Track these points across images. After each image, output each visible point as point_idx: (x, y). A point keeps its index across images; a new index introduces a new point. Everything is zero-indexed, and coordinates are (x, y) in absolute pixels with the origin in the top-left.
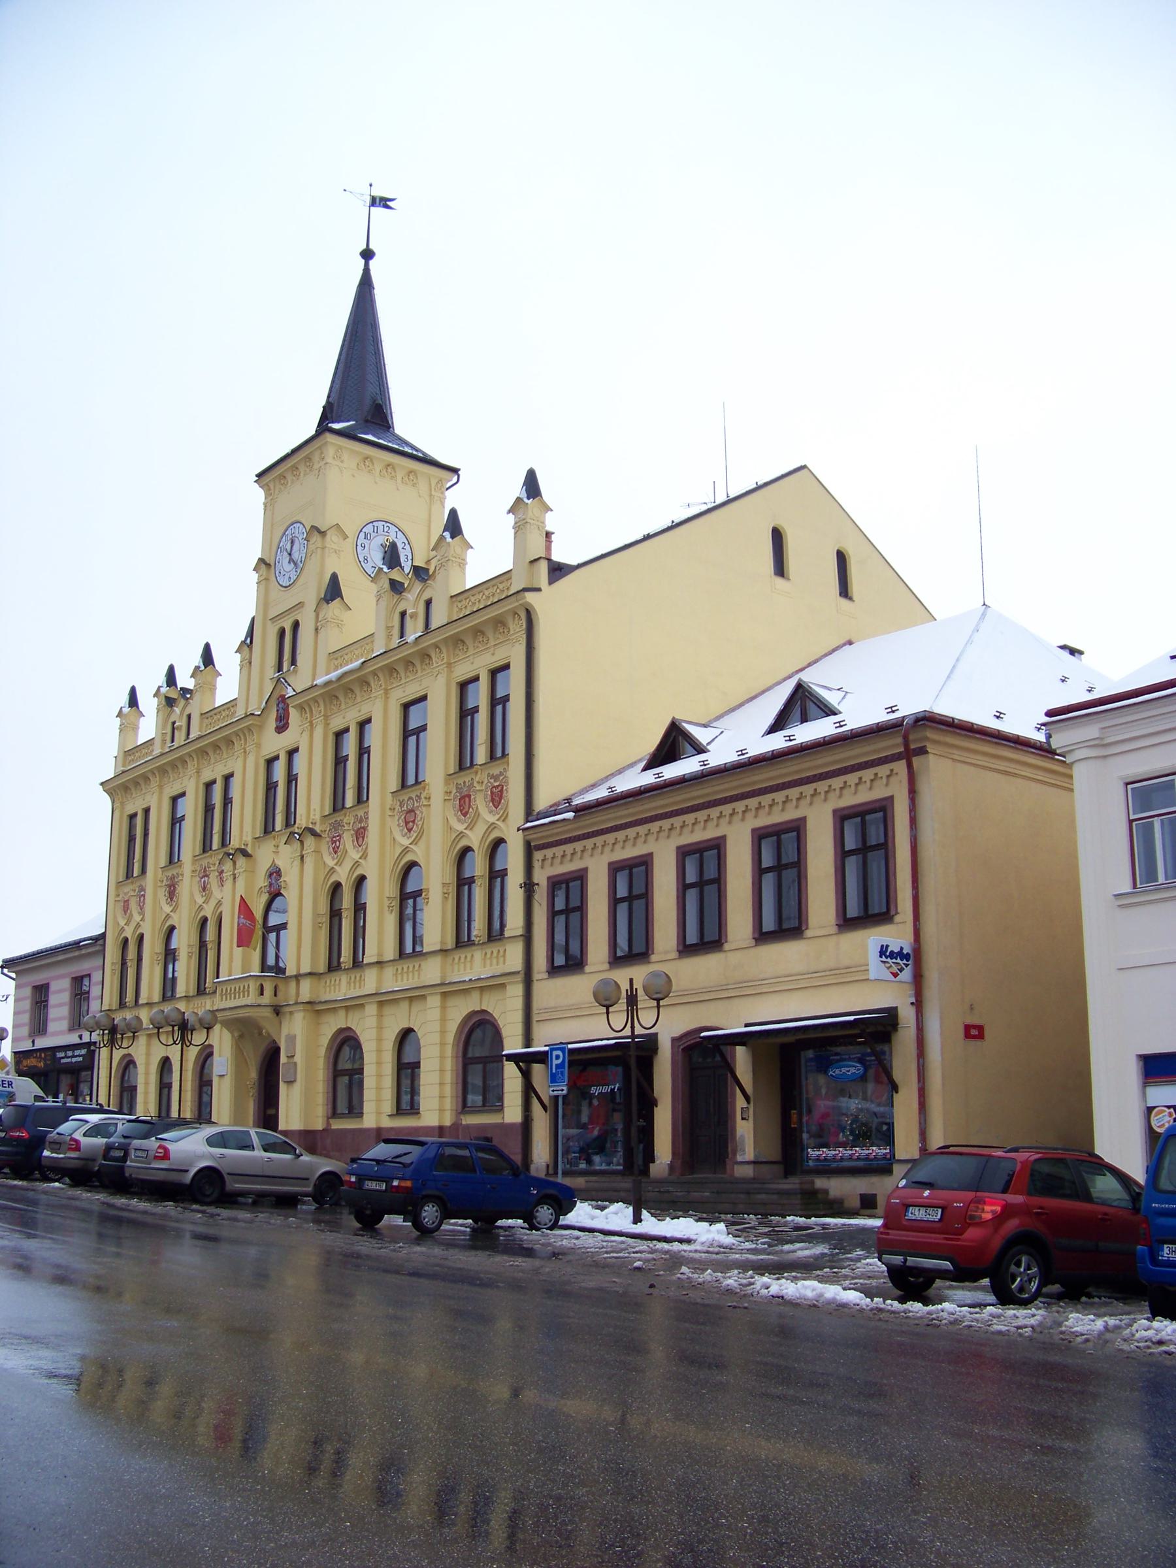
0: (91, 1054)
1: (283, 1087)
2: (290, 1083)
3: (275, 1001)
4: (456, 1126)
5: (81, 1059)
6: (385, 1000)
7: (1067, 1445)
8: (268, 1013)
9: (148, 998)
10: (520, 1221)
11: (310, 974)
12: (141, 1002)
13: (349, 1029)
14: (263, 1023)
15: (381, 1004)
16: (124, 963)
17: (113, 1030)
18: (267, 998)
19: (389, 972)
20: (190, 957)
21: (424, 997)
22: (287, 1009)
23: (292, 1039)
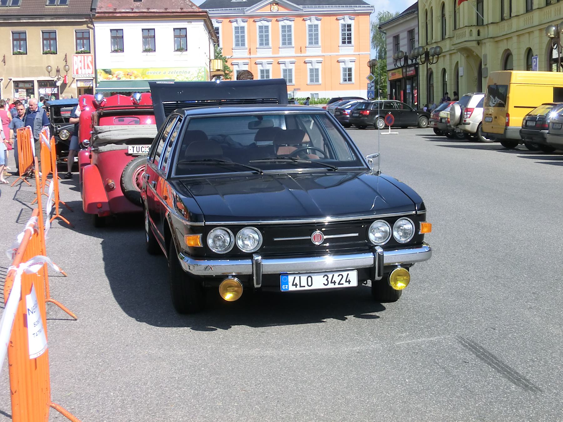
0: (417, 70)
1: (483, 79)
2: (486, 77)
3: (479, 38)
4: (254, 145)
5: (412, 72)
6: (520, 34)
7: (144, 196)
8: (474, 44)
9: (539, 4)
10: (499, 144)
11: (492, 23)
12: (512, 15)
13: (508, 49)
14: (473, 49)
15: (519, 36)
16: (443, 15)
17: (427, 54)
18: (475, 36)
19: (522, 19)
20: (450, 17)
21: (511, 37)
22: (484, 41)
23: (485, 56)
